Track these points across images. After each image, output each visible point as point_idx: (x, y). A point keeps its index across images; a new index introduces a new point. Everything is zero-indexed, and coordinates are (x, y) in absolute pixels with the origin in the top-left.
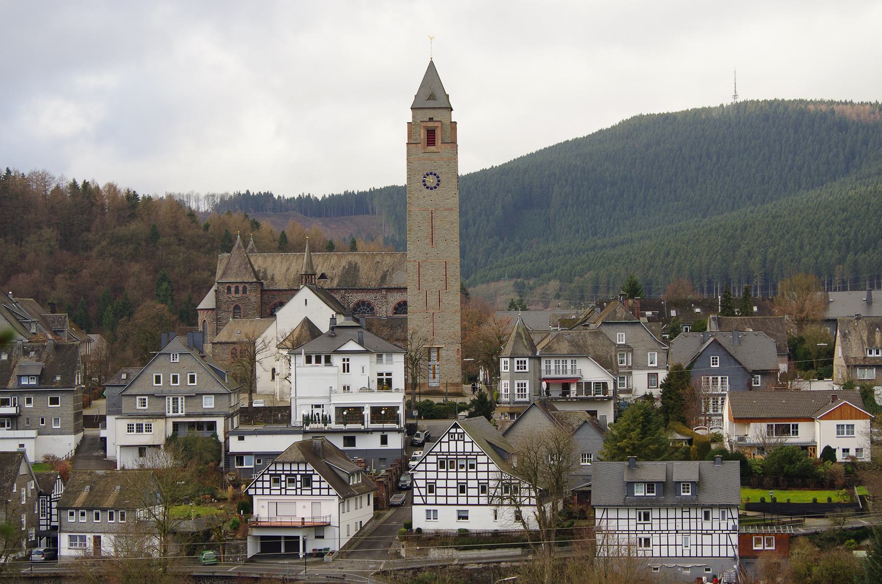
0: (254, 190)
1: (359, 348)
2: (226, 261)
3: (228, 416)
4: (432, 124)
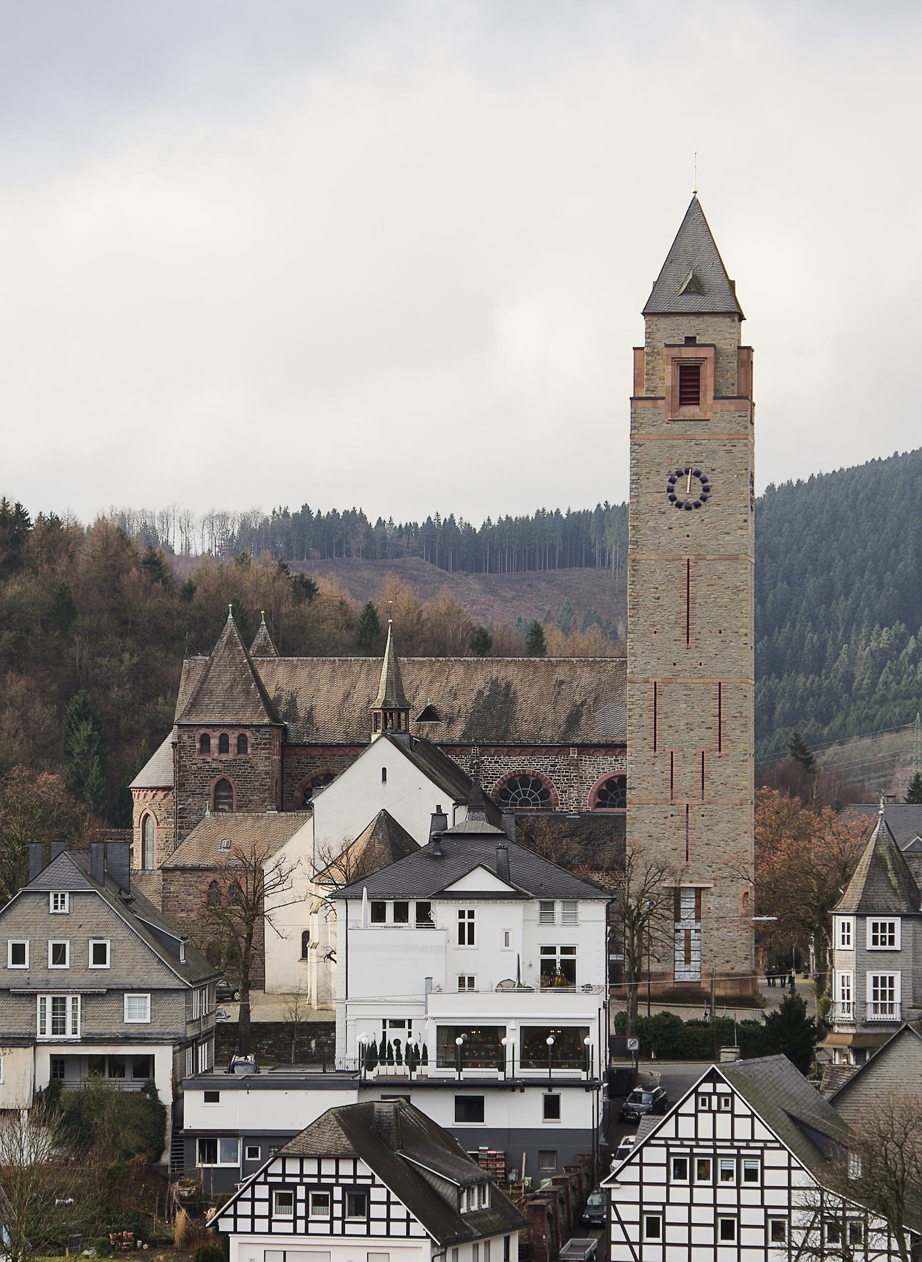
0: (322, 506)
1: (500, 886)
2: (197, 675)
3: (182, 1044)
4: (694, 352)
